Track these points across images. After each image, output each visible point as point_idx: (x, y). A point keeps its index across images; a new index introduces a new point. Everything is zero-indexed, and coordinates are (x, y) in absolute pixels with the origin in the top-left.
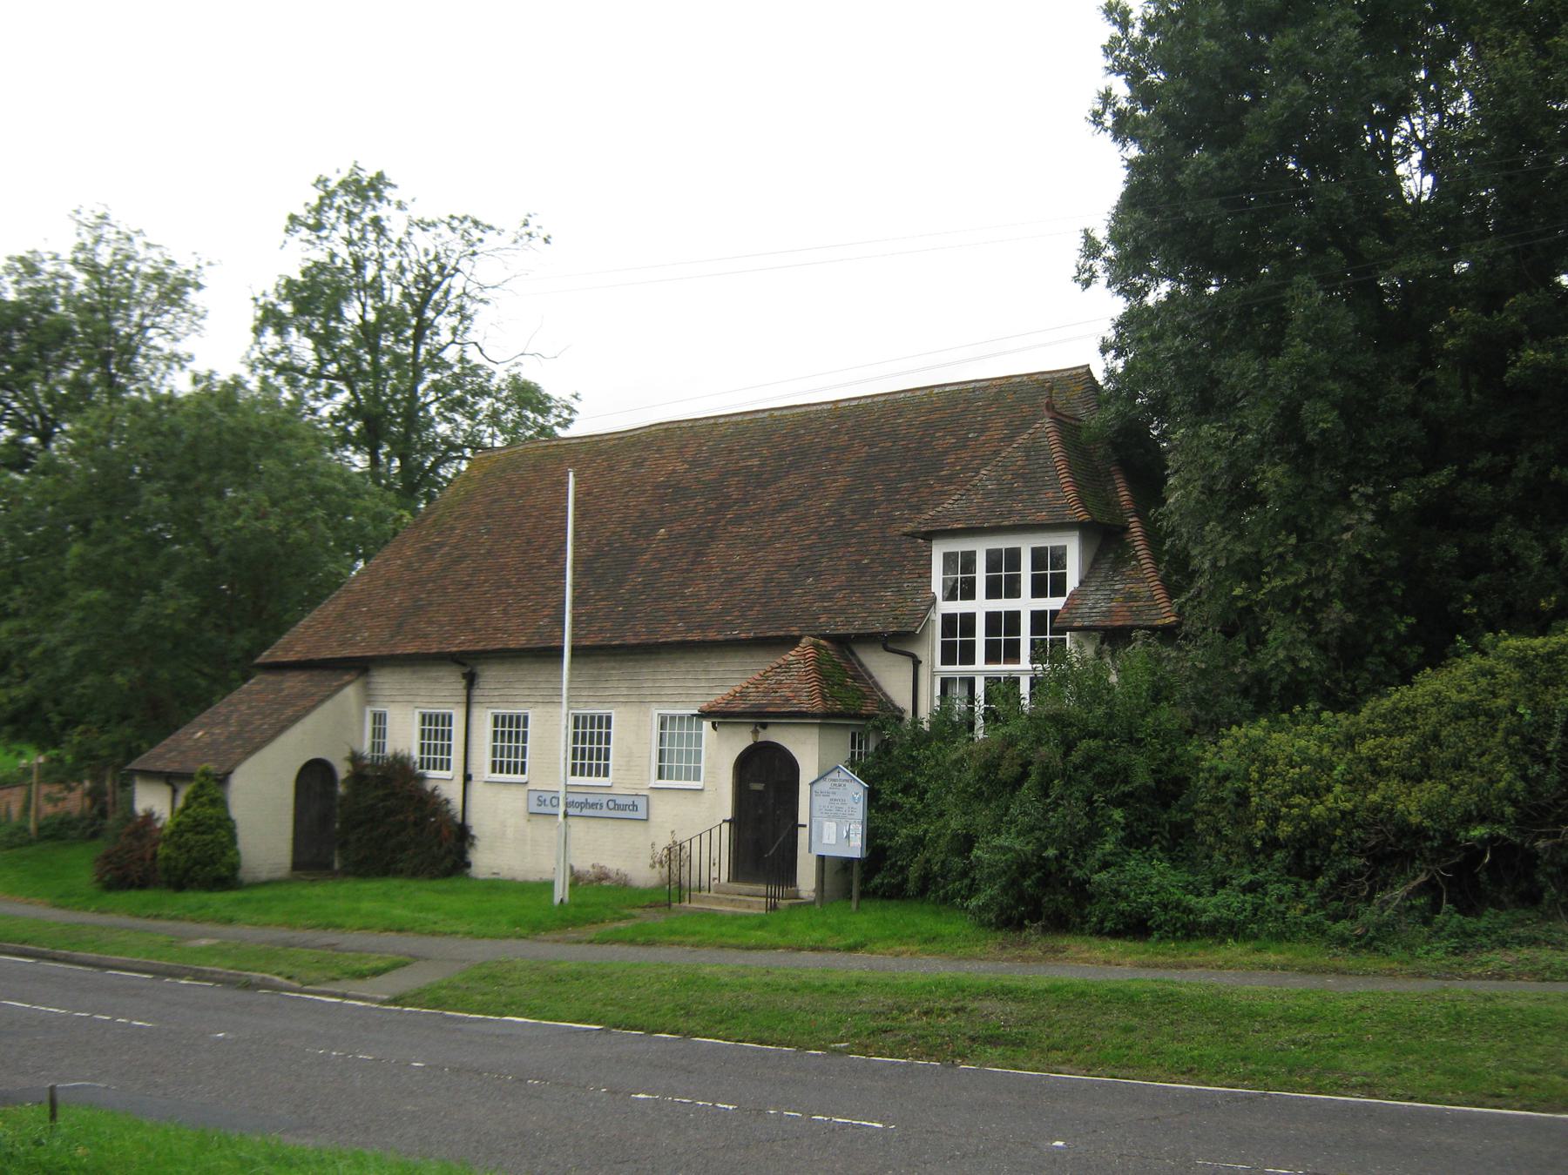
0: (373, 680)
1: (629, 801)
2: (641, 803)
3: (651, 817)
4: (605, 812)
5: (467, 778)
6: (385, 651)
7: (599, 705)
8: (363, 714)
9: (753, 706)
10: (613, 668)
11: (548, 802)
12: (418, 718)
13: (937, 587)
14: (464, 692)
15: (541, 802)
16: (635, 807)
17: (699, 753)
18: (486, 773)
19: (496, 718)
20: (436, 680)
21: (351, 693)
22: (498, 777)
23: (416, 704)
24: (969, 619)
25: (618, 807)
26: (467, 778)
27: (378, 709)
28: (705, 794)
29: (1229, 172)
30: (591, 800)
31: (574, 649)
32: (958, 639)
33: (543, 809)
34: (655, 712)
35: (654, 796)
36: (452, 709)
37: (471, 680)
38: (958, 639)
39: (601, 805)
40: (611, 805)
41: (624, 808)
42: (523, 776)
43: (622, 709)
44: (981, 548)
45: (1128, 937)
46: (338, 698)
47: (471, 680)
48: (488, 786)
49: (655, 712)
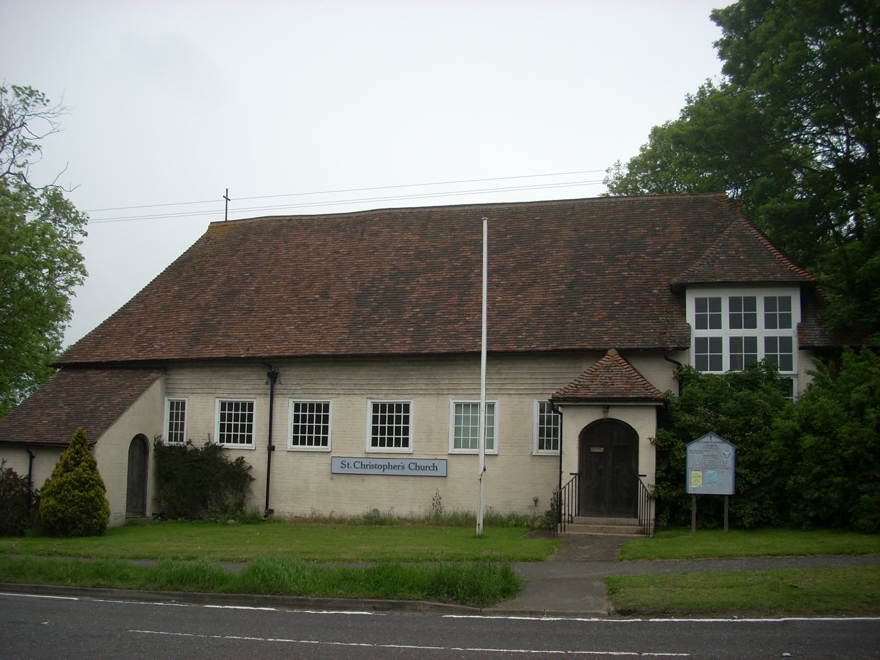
0: (172, 377)
1: (430, 464)
2: (441, 466)
3: (450, 475)
4: (407, 471)
5: (271, 449)
6: (185, 355)
7: (399, 396)
8: (163, 402)
9: (599, 394)
10: (412, 371)
11: (351, 465)
12: (218, 406)
13: (691, 316)
14: (269, 386)
15: (344, 465)
16: (435, 468)
17: (171, 428)
18: (290, 445)
19: (172, 403)
20: (238, 378)
21: (157, 387)
22: (299, 447)
23: (217, 395)
24: (717, 343)
25: (418, 467)
26: (271, 449)
27: (175, 398)
28: (499, 458)
29: (692, 104)
30: (392, 463)
31: (489, 353)
32: (709, 354)
33: (346, 471)
34: (452, 402)
35: (452, 461)
36: (255, 398)
37: (273, 378)
38: (709, 354)
39: (403, 467)
40: (357, 465)
41: (425, 468)
42: (555, 451)
43: (422, 399)
44: (725, 298)
45: (349, 519)
46: (151, 389)
47: (273, 378)
48: (290, 454)
49: (452, 402)
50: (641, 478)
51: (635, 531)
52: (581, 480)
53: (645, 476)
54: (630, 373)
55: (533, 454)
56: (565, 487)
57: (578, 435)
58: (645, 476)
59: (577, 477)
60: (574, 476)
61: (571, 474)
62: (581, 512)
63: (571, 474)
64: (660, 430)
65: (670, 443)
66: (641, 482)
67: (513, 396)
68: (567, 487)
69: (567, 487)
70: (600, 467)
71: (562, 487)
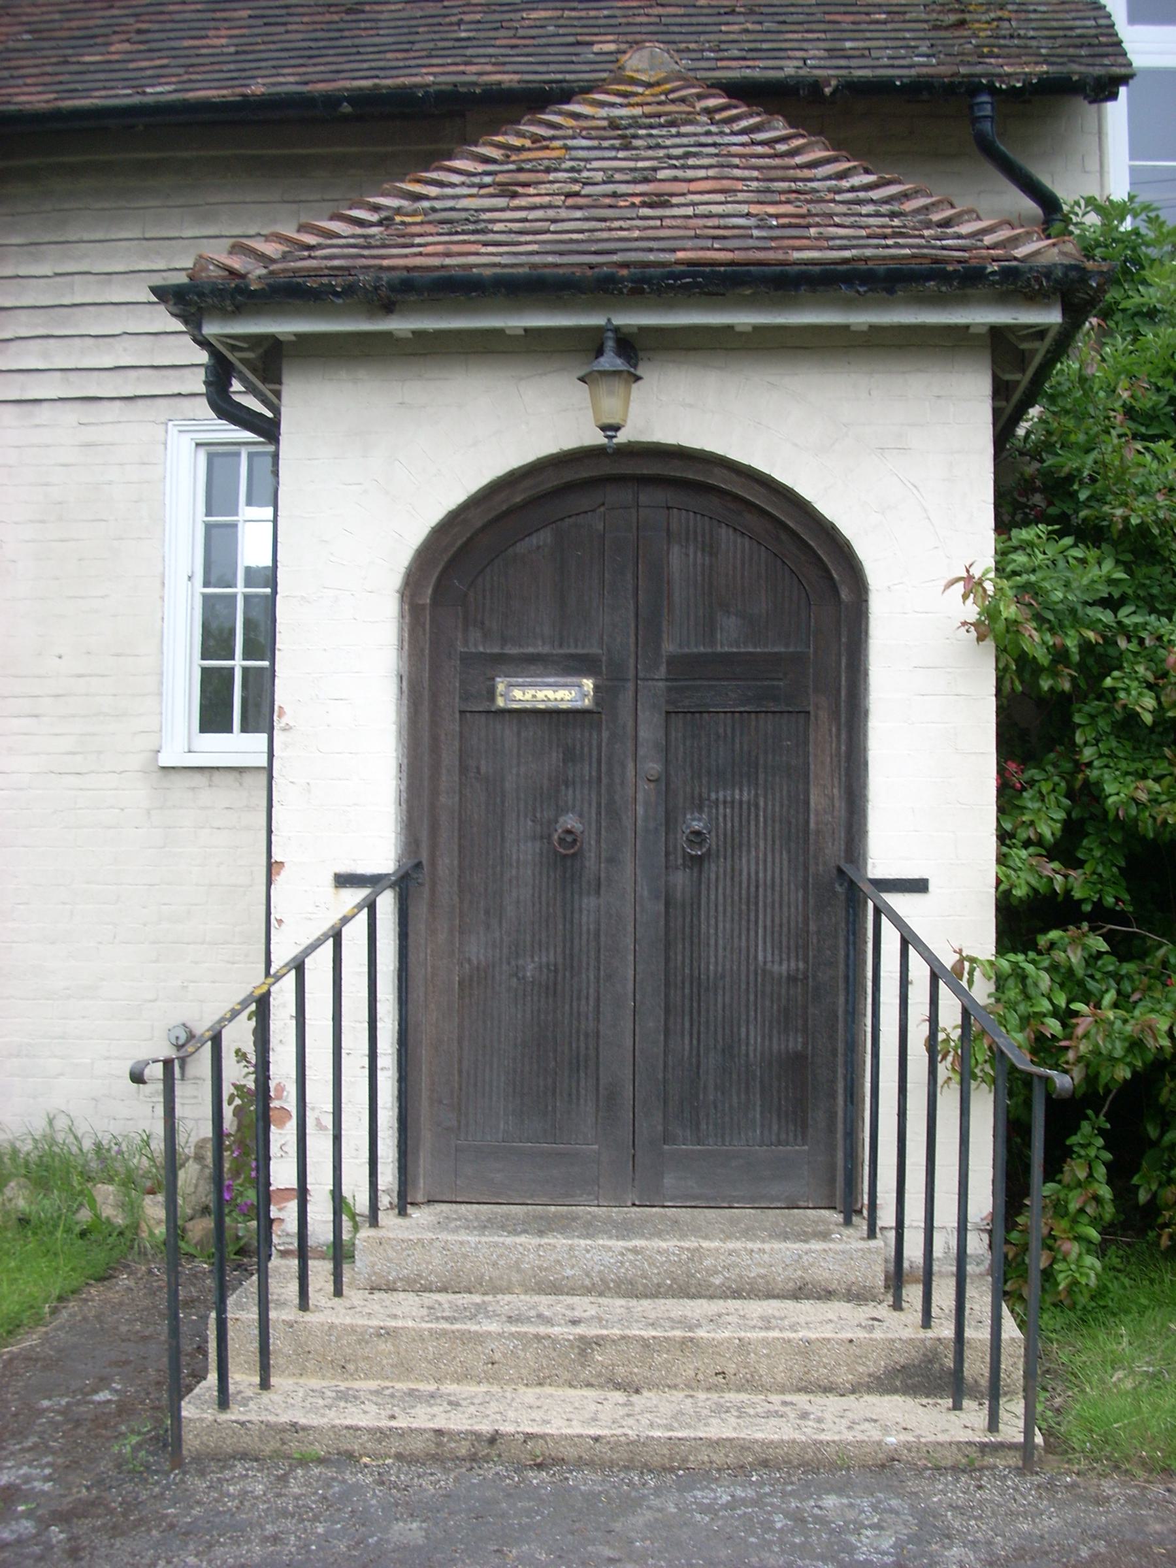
50: (895, 900)
51: (877, 1364)
52: (419, 927)
53: (919, 886)
54: (781, 147)
55: (165, 760)
56: (299, 967)
57: (404, 557)
58: (919, 886)
59: (387, 903)
60: (358, 895)
61: (344, 881)
62: (423, 1163)
63: (344, 881)
64: (1025, 534)
65: (1091, 635)
66: (908, 940)
67: (44, 413)
68: (319, 967)
69: (319, 967)
70: (570, 821)
71: (282, 955)
